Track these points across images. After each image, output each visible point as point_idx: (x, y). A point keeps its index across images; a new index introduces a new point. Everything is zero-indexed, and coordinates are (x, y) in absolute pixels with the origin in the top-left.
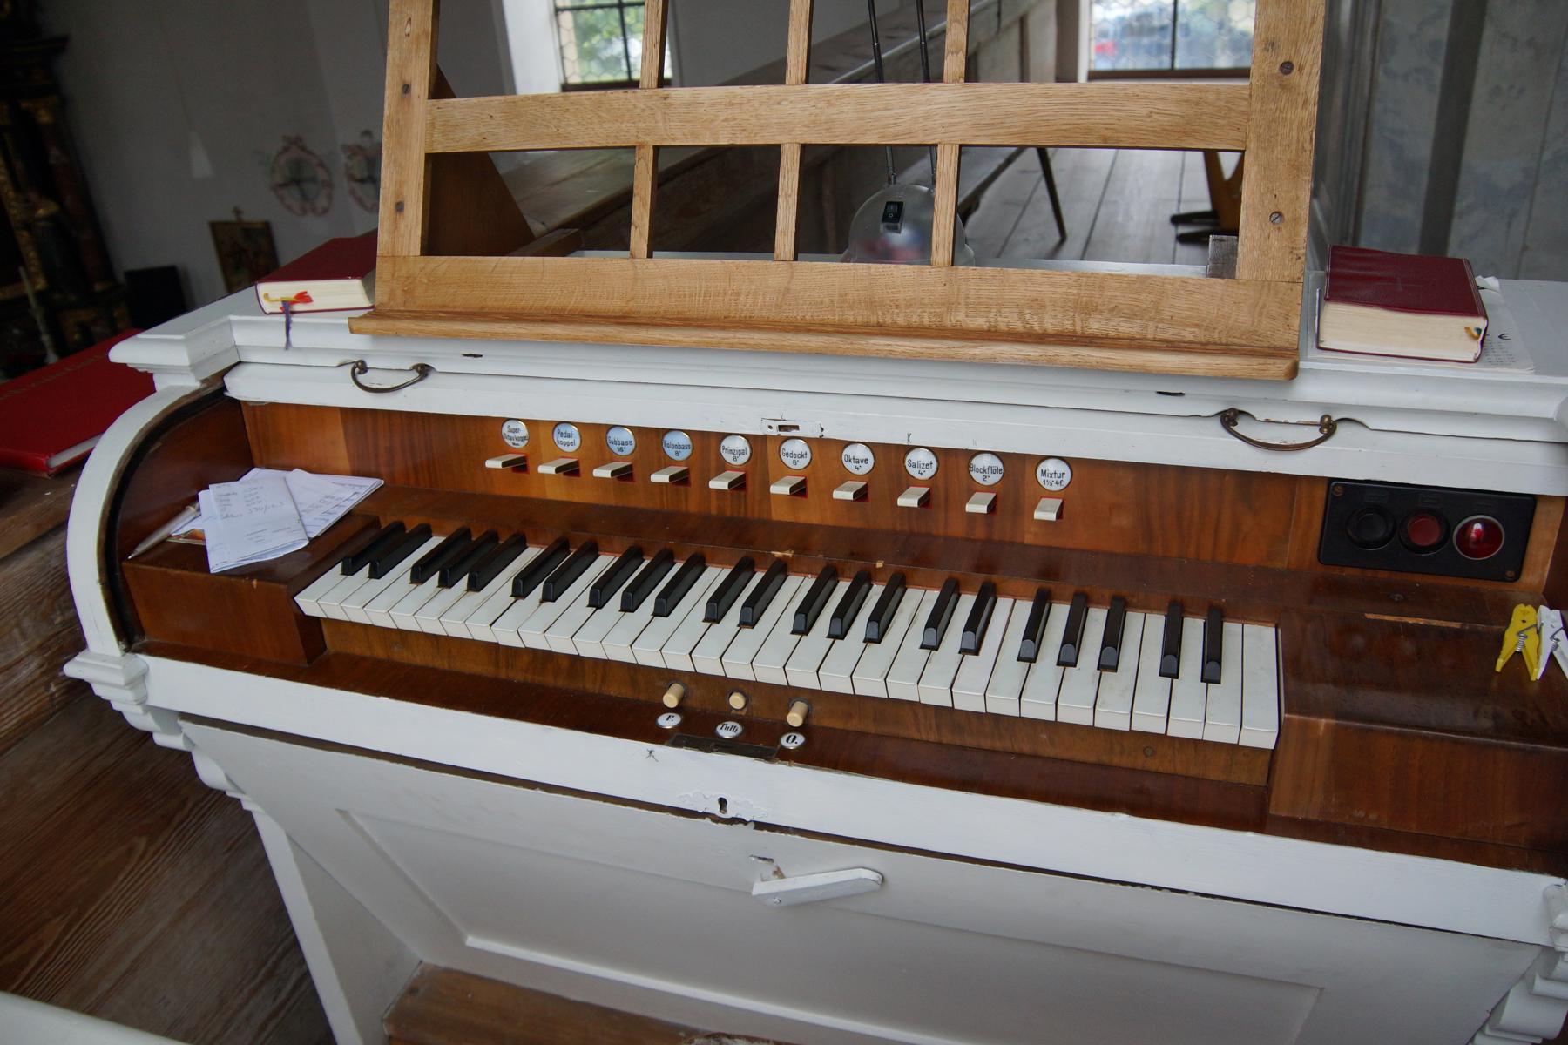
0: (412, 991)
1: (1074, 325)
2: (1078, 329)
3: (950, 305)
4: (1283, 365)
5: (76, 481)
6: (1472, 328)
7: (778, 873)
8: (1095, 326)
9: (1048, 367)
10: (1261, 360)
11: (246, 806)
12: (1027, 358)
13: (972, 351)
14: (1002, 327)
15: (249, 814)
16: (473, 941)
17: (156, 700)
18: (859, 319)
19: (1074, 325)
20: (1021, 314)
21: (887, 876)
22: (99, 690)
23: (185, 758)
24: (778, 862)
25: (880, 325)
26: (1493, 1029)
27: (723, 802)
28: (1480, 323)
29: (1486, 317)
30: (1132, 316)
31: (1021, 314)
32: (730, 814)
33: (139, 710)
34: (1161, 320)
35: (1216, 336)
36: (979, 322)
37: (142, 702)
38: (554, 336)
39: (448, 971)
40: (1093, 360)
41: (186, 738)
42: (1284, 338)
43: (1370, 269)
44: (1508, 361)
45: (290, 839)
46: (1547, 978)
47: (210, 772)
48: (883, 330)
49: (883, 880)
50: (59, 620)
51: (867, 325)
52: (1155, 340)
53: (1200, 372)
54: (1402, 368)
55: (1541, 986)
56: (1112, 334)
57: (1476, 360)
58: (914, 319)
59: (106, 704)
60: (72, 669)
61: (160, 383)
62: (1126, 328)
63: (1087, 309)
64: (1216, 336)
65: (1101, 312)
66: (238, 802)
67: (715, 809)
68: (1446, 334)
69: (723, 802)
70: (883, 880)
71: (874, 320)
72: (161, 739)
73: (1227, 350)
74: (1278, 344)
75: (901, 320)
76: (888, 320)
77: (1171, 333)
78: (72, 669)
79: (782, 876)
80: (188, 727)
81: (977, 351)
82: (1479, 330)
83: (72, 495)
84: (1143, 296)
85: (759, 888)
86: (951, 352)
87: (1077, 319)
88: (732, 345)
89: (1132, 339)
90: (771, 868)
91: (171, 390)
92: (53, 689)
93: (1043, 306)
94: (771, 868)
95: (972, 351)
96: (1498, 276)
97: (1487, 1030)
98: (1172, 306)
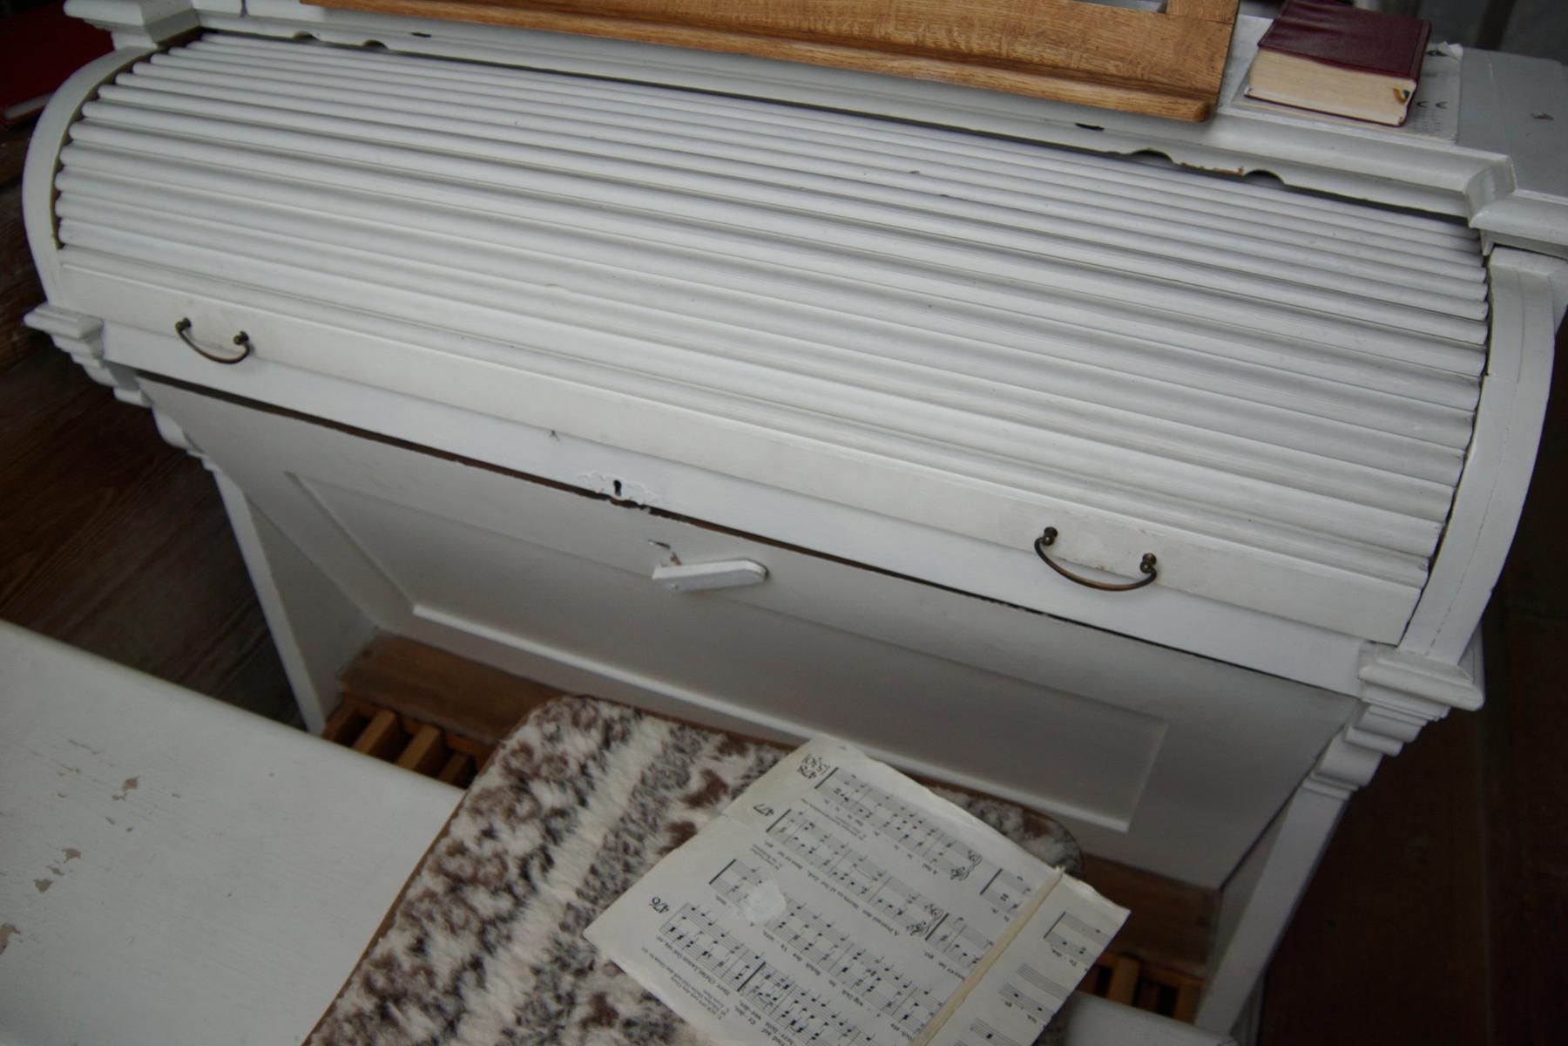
0: (366, 653)
1: (999, 47)
2: (1004, 52)
3: (881, 17)
4: (1193, 107)
5: (30, 135)
6: (1401, 89)
7: (675, 559)
8: (1021, 50)
9: (964, 86)
10: (1172, 99)
11: (209, 465)
12: (944, 75)
13: (890, 64)
14: (929, 43)
15: (210, 475)
16: (420, 611)
17: (113, 355)
18: (792, 23)
19: (999, 47)
20: (950, 31)
21: (773, 572)
22: (60, 343)
23: (145, 415)
24: (676, 549)
25: (811, 31)
26: (1320, 774)
27: (618, 485)
28: (1410, 86)
29: (1417, 80)
30: (1057, 43)
31: (950, 31)
32: (624, 496)
33: (96, 363)
34: (1087, 50)
35: (1139, 71)
36: (908, 37)
37: (99, 356)
38: (493, 19)
39: (400, 639)
40: (1007, 83)
41: (145, 396)
42: (1206, 80)
43: (1321, 20)
44: (1434, 130)
45: (249, 500)
46: (1357, 728)
47: (170, 430)
48: (813, 37)
49: (767, 574)
50: (18, 272)
51: (799, 30)
52: (1078, 70)
53: (1111, 106)
54: (1323, 125)
55: (1352, 735)
56: (1036, 59)
57: (1401, 125)
58: (845, 28)
59: (67, 356)
60: (33, 320)
61: (120, 42)
62: (1052, 55)
63: (1015, 32)
64: (1139, 71)
65: (1028, 36)
66: (199, 462)
67: (611, 491)
68: (1377, 95)
69: (618, 485)
70: (767, 574)
71: (805, 25)
72: (123, 395)
73: (1146, 86)
74: (1199, 85)
75: (831, 28)
76: (819, 26)
77: (1095, 65)
78: (33, 320)
79: (679, 563)
80: (146, 384)
81: (895, 64)
82: (1407, 93)
83: (25, 149)
84: (1072, 24)
85: (659, 573)
86: (871, 63)
87: (1004, 41)
88: (661, 40)
89: (1055, 67)
90: (667, 556)
91: (129, 50)
92: (15, 338)
93: (971, 25)
94: (667, 556)
95: (890, 64)
96: (1464, 44)
97: (1312, 775)
98: (1100, 36)
